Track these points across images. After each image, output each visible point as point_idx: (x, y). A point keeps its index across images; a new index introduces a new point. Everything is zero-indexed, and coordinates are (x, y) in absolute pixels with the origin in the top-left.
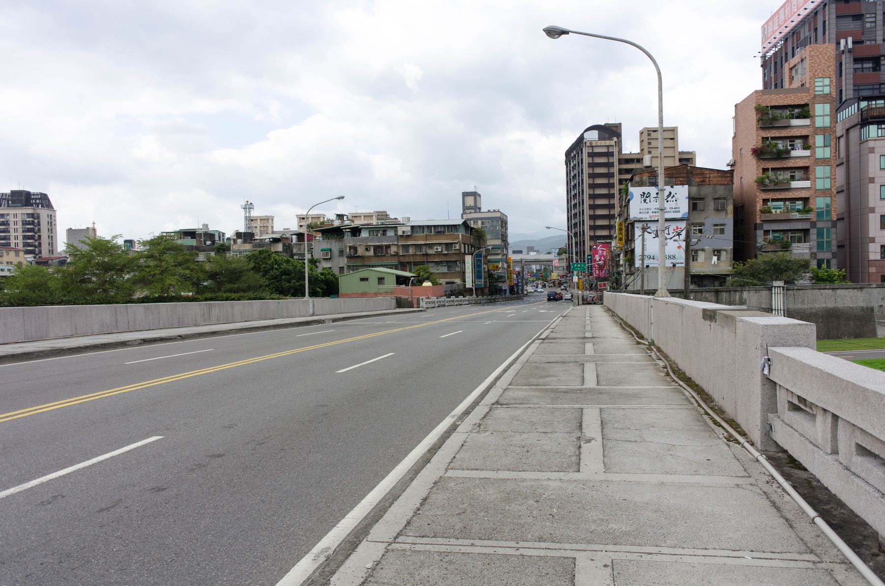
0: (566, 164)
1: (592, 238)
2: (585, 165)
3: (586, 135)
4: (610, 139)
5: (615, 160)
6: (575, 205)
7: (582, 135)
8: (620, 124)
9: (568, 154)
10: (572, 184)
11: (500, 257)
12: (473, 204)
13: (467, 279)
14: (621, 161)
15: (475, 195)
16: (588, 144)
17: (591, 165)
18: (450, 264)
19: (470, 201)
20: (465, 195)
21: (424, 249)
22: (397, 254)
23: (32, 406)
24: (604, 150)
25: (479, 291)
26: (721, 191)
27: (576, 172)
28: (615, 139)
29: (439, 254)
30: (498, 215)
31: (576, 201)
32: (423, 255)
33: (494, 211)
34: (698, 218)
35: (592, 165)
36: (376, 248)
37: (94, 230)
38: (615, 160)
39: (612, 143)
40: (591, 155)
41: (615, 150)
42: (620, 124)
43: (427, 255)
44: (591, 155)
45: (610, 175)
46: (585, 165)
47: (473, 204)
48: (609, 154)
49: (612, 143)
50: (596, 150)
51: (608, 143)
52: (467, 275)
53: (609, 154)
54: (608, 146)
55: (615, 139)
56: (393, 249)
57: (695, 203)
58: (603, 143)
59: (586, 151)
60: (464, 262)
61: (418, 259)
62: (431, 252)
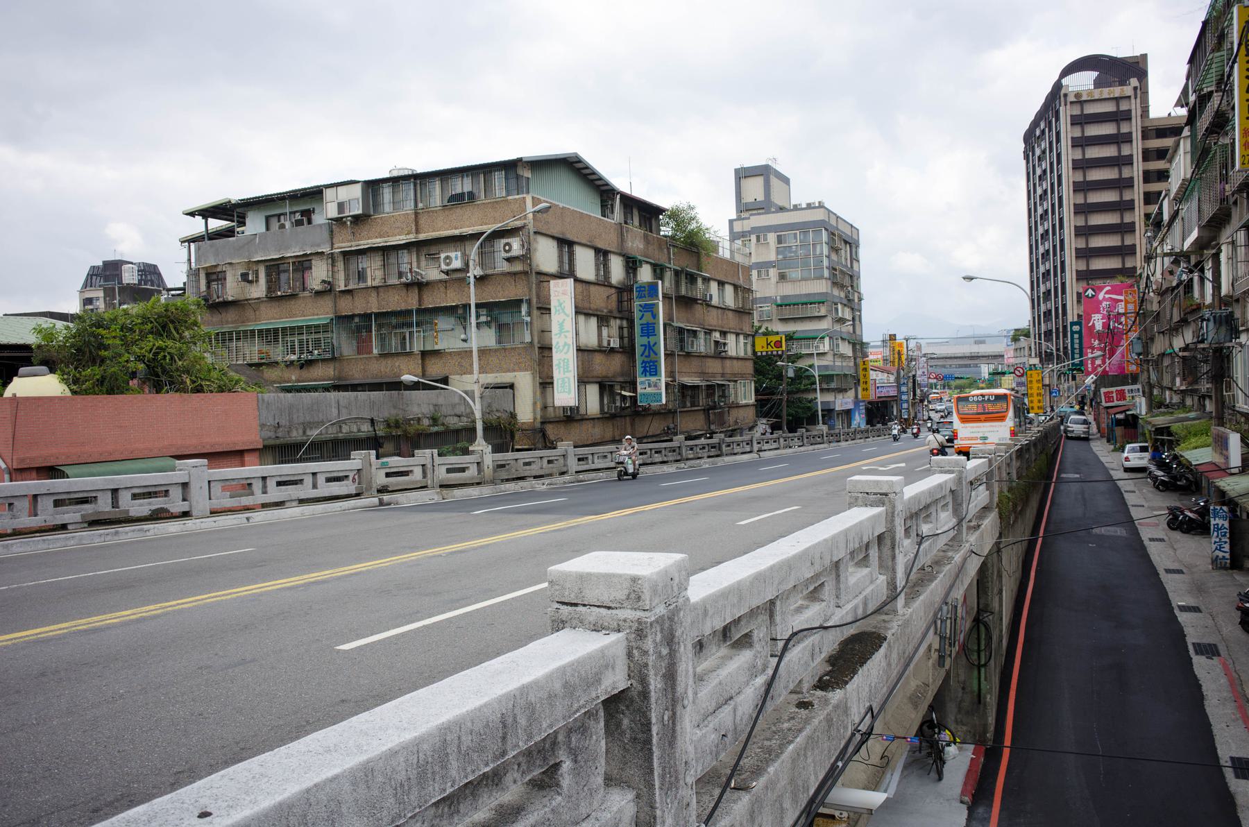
0: (1026, 157)
1: (1083, 276)
2: (1069, 232)
3: (1065, 81)
4: (1123, 83)
5: (1135, 127)
6: (1047, 274)
7: (1058, 86)
8: (1144, 57)
9: (1030, 138)
10: (1041, 250)
11: (824, 325)
12: (761, 198)
13: (557, 375)
14: (1146, 135)
15: (764, 172)
16: (1071, 98)
17: (1078, 143)
18: (498, 313)
19: (754, 190)
20: (742, 175)
21: (407, 261)
22: (328, 290)
23: (205, 605)
24: (1109, 108)
25: (624, 414)
27: (1047, 205)
28: (1134, 82)
29: (456, 278)
30: (818, 215)
31: (1049, 265)
32: (408, 286)
33: (809, 206)
35: (1080, 165)
36: (274, 268)
37: (870, 403)
38: (1135, 127)
39: (1128, 90)
40: (1077, 121)
41: (1134, 106)
42: (1144, 57)
43: (420, 286)
44: (1077, 121)
45: (1123, 161)
46: (1069, 232)
47: (761, 198)
48: (1121, 117)
49: (1128, 90)
50: (1090, 109)
51: (1117, 91)
52: (557, 356)
53: (1121, 117)
54: (1117, 100)
55: (1134, 82)
56: (319, 273)
58: (1105, 92)
59: (1065, 113)
60: (545, 309)
61: (396, 301)
62: (432, 273)
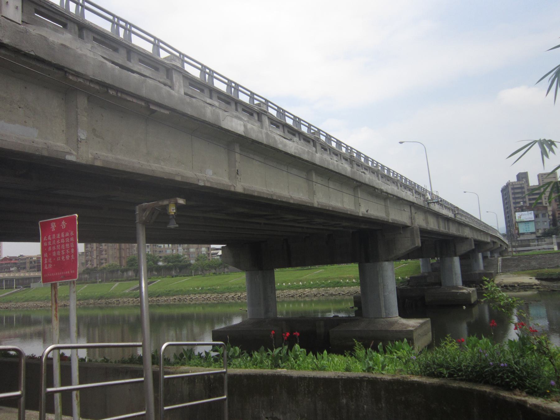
26: (544, 212)
34: (538, 220)
41: (525, 186)
46: (510, 194)
57: (536, 216)
